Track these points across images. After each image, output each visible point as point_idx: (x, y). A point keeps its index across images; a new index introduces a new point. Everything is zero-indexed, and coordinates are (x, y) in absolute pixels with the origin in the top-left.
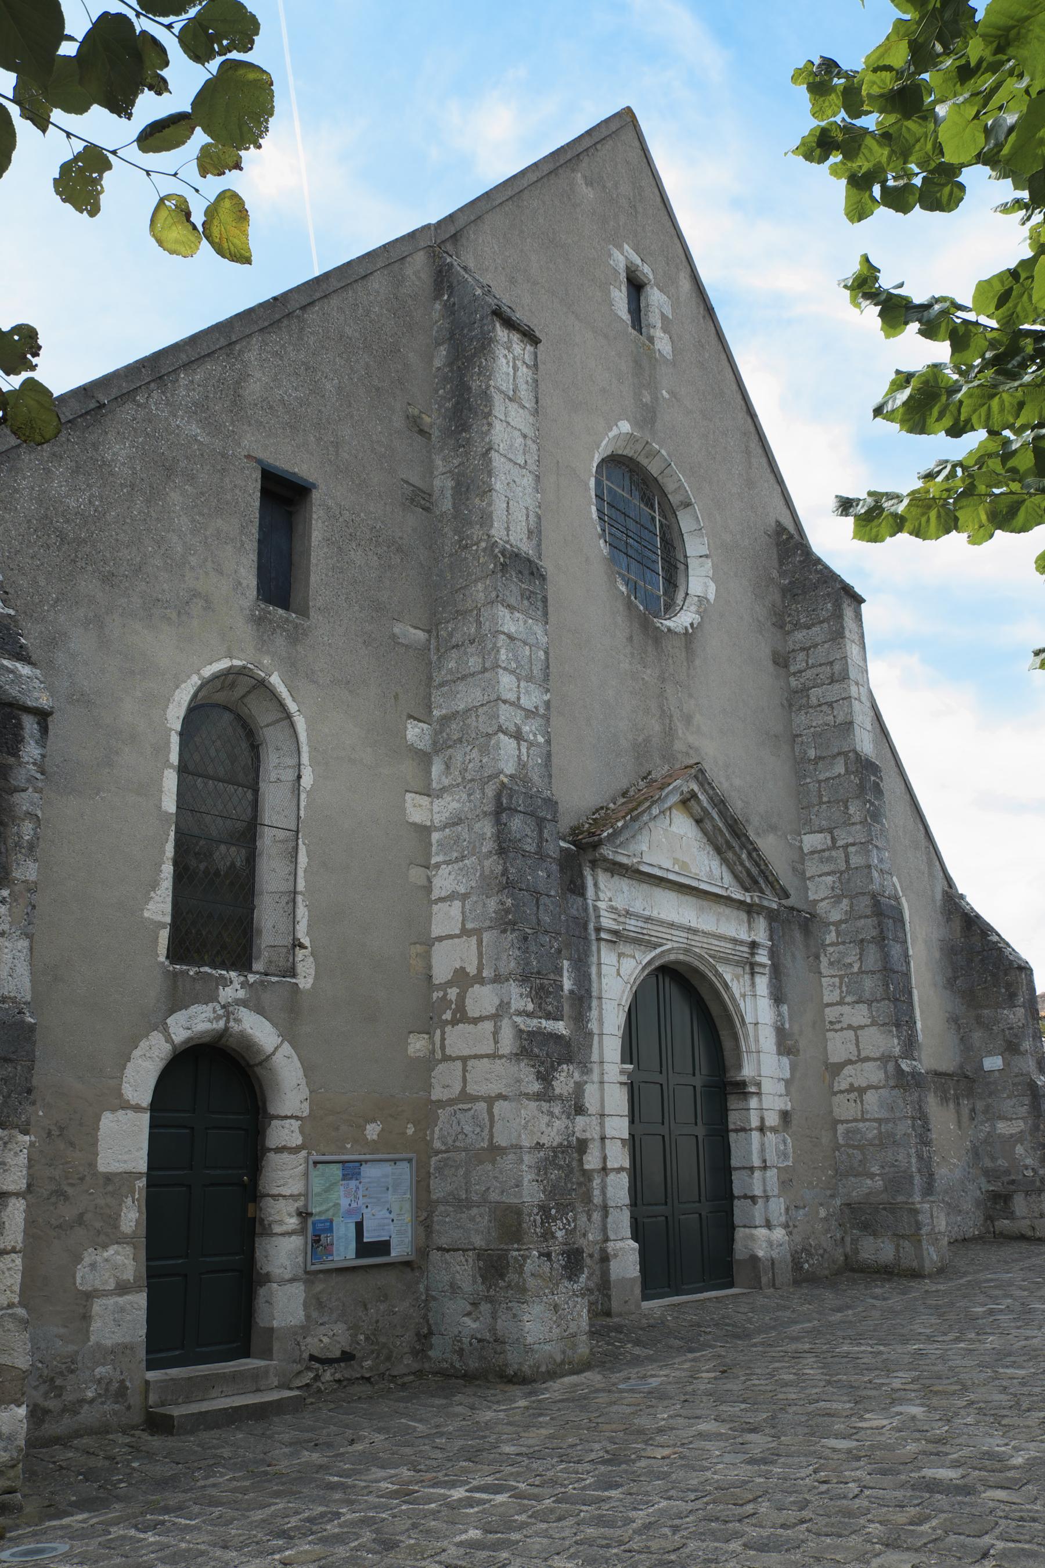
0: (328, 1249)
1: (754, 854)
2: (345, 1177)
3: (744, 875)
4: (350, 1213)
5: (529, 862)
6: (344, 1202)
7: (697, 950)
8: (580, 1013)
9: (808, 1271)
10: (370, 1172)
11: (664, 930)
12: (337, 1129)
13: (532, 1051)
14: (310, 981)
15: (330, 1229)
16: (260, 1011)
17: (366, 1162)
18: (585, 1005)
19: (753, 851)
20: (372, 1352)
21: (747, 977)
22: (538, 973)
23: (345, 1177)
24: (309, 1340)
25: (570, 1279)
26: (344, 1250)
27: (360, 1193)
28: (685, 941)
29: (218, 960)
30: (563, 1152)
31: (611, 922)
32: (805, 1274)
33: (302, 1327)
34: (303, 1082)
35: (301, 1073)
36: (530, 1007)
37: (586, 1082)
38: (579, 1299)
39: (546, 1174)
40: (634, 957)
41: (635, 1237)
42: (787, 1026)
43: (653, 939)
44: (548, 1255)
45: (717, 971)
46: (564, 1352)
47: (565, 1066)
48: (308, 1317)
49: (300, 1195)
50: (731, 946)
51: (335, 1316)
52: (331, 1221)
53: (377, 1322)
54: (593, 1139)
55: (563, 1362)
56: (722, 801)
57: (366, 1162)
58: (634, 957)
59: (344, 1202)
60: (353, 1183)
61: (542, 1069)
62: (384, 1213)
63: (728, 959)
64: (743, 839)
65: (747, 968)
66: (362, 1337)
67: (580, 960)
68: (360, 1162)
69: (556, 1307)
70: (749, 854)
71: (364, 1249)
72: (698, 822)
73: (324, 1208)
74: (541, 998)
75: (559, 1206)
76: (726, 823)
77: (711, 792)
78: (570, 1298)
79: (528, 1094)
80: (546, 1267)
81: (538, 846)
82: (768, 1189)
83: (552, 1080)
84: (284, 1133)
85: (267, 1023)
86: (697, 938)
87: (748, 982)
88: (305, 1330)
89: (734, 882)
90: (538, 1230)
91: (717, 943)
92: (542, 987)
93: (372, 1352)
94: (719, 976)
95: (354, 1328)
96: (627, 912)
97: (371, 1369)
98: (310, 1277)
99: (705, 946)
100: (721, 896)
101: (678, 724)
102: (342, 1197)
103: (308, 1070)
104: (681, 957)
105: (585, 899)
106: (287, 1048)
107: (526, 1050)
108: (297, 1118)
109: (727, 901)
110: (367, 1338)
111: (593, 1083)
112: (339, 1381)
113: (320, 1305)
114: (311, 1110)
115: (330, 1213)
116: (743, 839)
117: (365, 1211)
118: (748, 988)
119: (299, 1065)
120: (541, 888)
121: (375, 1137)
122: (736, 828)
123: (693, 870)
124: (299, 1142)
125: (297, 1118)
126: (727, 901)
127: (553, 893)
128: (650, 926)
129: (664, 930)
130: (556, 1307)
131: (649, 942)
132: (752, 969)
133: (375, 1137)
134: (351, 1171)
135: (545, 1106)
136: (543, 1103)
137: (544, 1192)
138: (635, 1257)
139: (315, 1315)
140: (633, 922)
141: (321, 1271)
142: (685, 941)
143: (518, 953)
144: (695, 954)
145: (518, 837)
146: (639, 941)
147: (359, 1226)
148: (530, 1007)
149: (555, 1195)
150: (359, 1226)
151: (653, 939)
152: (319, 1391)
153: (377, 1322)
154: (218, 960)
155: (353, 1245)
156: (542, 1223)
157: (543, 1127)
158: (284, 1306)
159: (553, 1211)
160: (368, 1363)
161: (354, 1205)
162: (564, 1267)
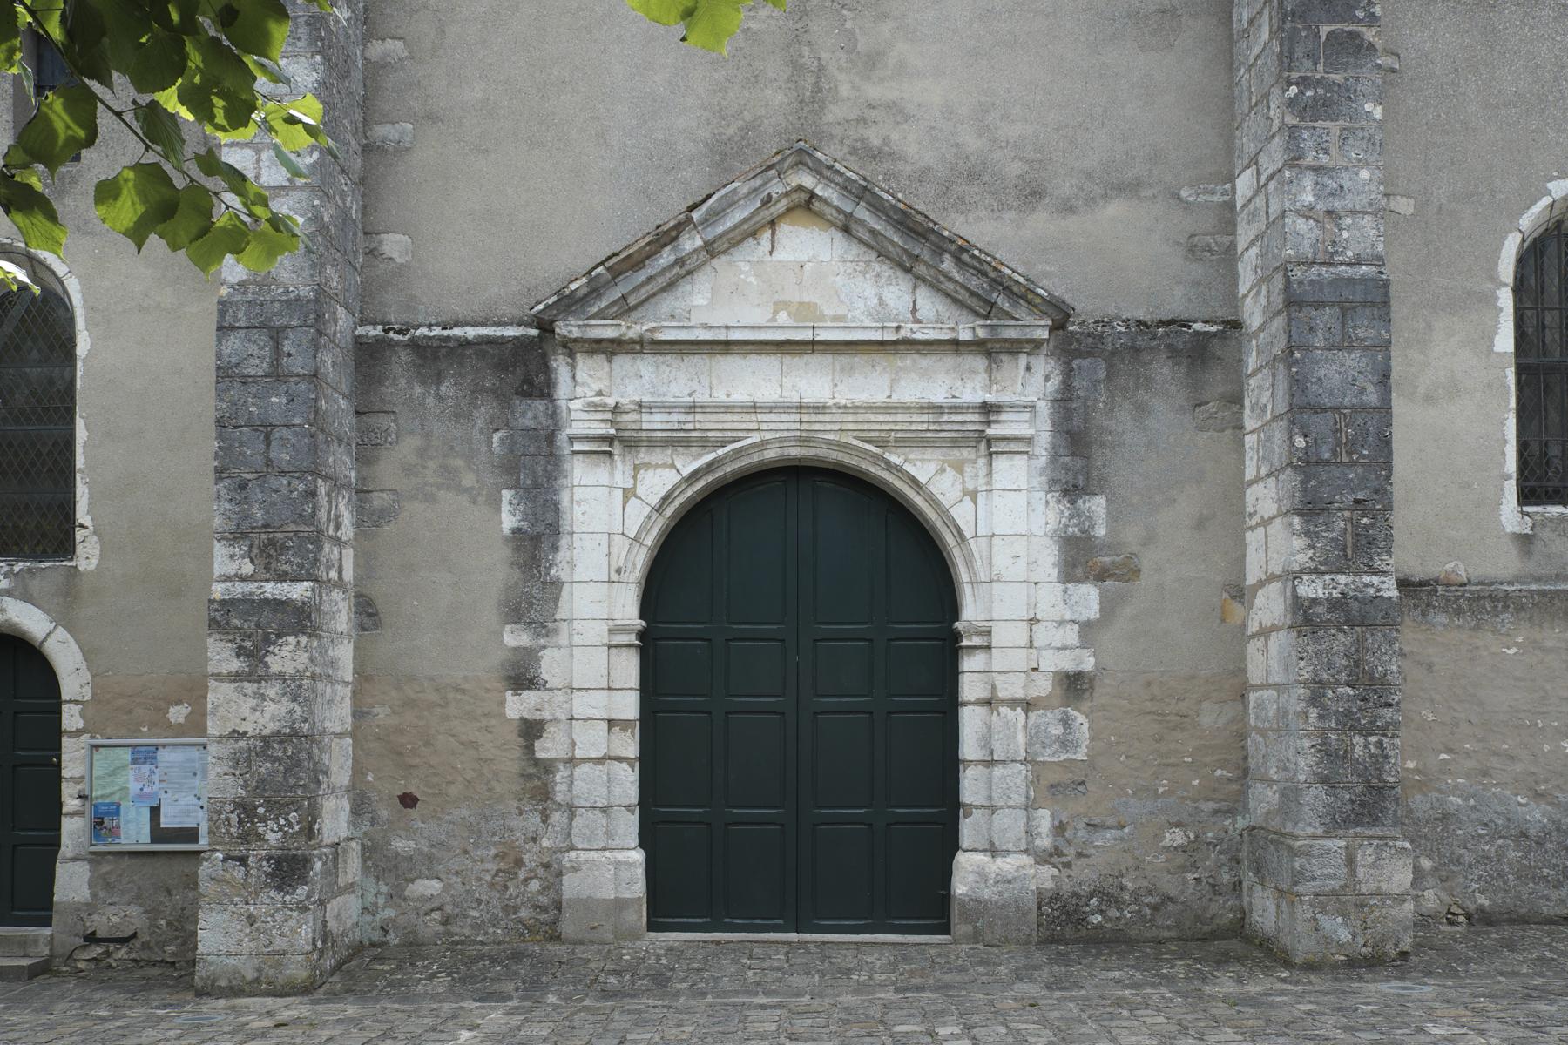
0: (114, 832)
1: (965, 257)
2: (134, 761)
3: (963, 295)
4: (141, 797)
5: (254, 390)
6: (134, 787)
7: (831, 436)
8: (534, 557)
9: (1099, 926)
10: (165, 756)
11: (736, 417)
12: (130, 712)
13: (228, 623)
14: (94, 562)
15: (117, 813)
16: (27, 598)
17: (164, 746)
18: (546, 546)
19: (961, 252)
20: (177, 938)
21: (982, 461)
22: (266, 526)
23: (134, 761)
24: (95, 917)
25: (279, 889)
26: (134, 832)
27: (156, 778)
28: (797, 426)
29: (39, 549)
30: (281, 742)
31: (595, 425)
32: (1069, 930)
33: (87, 904)
34: (84, 666)
35: (79, 657)
36: (248, 568)
37: (545, 647)
38: (295, 914)
39: (249, 766)
40: (673, 466)
41: (643, 843)
42: (1101, 531)
43: (710, 434)
44: (243, 861)
45: (888, 463)
46: (259, 970)
47: (291, 639)
48: (94, 896)
49: (83, 778)
50: (931, 418)
51: (126, 898)
52: (119, 805)
53: (183, 909)
54: (556, 720)
55: (257, 980)
56: (865, 188)
57: (164, 746)
58: (673, 466)
59: (134, 787)
60: (146, 768)
61: (248, 644)
62: (192, 799)
63: (923, 440)
64: (933, 238)
65: (983, 446)
66: (163, 922)
67: (536, 485)
68: (157, 747)
69: (251, 920)
70: (959, 261)
71: (158, 834)
72: (846, 230)
73: (108, 791)
74: (270, 556)
75: (269, 805)
76: (890, 220)
77: (840, 180)
78: (277, 910)
79: (219, 674)
80: (239, 872)
81: (271, 365)
82: (995, 795)
83: (265, 655)
84: (71, 718)
85: (36, 610)
86: (827, 418)
87: (983, 471)
88: (91, 908)
89: (955, 312)
90: (233, 830)
91: (881, 418)
92: (272, 543)
93: (177, 938)
94: (889, 466)
95: (153, 912)
96: (640, 405)
97: (174, 954)
98: (96, 858)
99: (851, 427)
100: (882, 343)
101: (842, 77)
102: (132, 781)
103: (88, 653)
104: (795, 452)
105: (553, 401)
106: (61, 633)
107: (218, 623)
108: (77, 702)
109: (955, 346)
110: (169, 924)
111: (559, 647)
112: (134, 960)
113: (109, 887)
114: (94, 694)
115: (115, 799)
116: (933, 238)
117: (163, 796)
118: (982, 480)
119: (76, 648)
120: (275, 417)
121: (181, 720)
122: (910, 224)
123: (828, 312)
124: (81, 725)
125: (77, 702)
126: (955, 346)
127: (297, 421)
128: (699, 417)
129: (736, 417)
130: (251, 920)
131: (706, 439)
132: (989, 446)
133: (181, 720)
134: (145, 755)
135: (250, 687)
136: (246, 684)
137: (244, 787)
138: (640, 873)
139: (102, 894)
140: (658, 417)
141: (110, 853)
142: (797, 426)
143: (227, 506)
144: (829, 442)
145: (234, 360)
146: (677, 442)
147: (155, 812)
148: (248, 568)
149: (265, 790)
150: (155, 812)
151: (710, 434)
152: (110, 966)
153: (183, 909)
154: (39, 549)
155: (147, 830)
156: (240, 821)
157: (246, 712)
158: (72, 882)
159: (261, 810)
160: (171, 948)
161: (147, 790)
162: (271, 875)
